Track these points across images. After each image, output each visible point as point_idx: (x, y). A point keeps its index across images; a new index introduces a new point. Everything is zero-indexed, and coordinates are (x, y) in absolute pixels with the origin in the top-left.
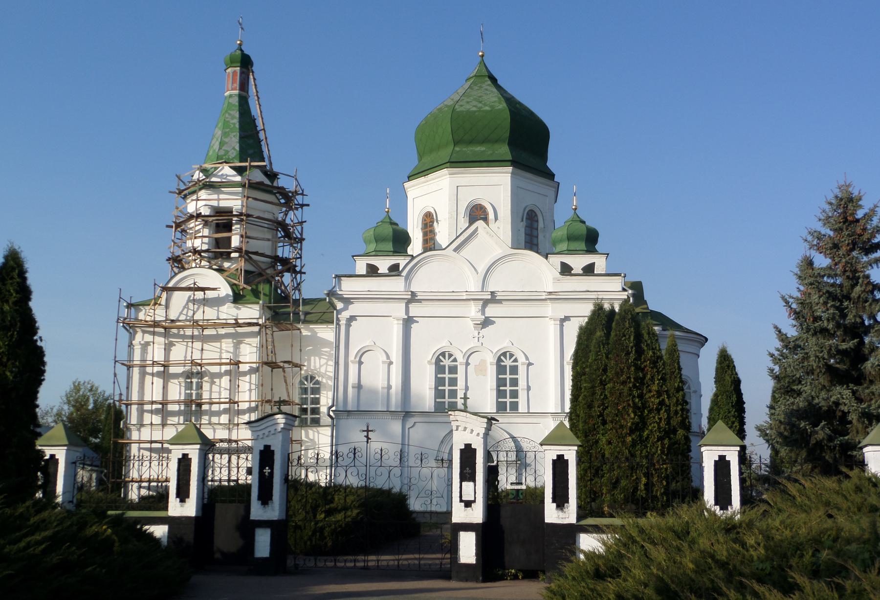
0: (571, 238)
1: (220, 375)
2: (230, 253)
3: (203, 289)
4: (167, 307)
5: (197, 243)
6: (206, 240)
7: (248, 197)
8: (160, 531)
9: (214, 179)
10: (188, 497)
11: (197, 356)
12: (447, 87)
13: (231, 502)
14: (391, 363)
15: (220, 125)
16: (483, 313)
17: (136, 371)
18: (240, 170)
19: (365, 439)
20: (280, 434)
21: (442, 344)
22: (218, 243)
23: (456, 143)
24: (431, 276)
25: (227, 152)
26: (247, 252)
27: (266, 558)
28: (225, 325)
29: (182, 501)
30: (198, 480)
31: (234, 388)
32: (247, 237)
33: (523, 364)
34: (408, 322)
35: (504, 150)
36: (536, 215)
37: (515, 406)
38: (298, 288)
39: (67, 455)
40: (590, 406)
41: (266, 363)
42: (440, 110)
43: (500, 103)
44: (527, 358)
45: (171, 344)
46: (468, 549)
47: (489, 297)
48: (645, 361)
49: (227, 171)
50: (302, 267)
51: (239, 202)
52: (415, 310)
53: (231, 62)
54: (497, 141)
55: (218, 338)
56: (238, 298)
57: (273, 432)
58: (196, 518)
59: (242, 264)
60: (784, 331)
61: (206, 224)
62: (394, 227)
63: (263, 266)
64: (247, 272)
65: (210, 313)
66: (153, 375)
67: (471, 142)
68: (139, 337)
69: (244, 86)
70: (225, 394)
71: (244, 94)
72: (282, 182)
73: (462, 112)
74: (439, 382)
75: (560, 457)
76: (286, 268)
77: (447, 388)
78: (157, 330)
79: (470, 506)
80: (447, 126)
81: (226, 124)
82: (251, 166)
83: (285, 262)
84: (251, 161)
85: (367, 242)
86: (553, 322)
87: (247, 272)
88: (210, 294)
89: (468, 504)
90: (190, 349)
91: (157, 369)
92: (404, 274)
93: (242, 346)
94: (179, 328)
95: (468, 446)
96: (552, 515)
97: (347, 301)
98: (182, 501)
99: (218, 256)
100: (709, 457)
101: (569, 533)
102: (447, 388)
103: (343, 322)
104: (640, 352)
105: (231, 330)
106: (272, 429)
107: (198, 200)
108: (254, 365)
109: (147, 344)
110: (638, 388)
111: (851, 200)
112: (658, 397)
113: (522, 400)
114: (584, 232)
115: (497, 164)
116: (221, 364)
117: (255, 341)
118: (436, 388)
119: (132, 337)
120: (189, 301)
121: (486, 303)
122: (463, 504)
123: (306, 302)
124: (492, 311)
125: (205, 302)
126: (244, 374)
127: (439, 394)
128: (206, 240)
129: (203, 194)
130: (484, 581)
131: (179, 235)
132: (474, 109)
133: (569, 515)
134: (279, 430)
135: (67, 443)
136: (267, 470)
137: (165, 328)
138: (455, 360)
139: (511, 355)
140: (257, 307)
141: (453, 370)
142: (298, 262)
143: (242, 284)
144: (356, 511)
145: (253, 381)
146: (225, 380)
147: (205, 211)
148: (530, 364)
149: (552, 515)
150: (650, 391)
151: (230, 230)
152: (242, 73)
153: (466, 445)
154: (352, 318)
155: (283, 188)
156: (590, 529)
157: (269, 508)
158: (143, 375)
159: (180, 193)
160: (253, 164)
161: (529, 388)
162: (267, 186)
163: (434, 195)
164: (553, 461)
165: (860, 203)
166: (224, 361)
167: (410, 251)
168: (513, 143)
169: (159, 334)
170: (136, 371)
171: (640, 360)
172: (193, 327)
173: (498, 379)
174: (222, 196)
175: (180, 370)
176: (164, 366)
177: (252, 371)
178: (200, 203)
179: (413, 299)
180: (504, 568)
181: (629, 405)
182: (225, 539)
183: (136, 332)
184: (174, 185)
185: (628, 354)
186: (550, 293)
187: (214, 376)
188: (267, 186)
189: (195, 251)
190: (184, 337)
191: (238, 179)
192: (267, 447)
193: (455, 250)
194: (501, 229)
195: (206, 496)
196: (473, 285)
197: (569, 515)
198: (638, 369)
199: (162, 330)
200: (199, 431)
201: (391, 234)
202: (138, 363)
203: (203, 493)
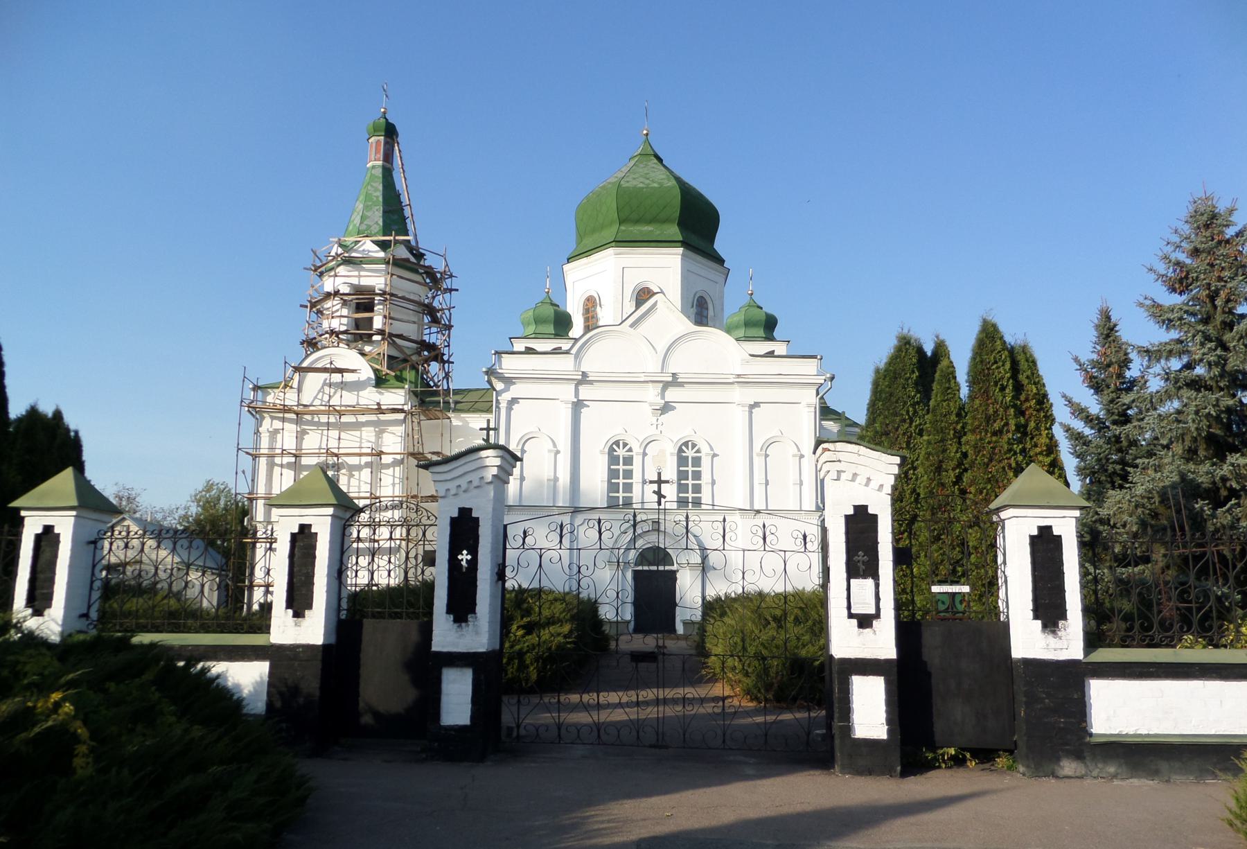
0: (748, 324)
1: (359, 468)
2: (372, 335)
4: (299, 390)
5: (336, 324)
6: (345, 321)
8: (246, 677)
9: (354, 255)
11: (333, 444)
12: (611, 167)
13: (397, 616)
14: (558, 452)
15: (362, 198)
16: (663, 397)
17: (263, 462)
18: (384, 245)
19: (655, 497)
20: (491, 487)
22: (358, 324)
24: (600, 357)
25: (369, 227)
26: (391, 335)
27: (463, 728)
28: (364, 411)
29: (298, 614)
30: (329, 575)
31: (375, 481)
32: (391, 318)
33: (707, 454)
34: (578, 405)
35: (674, 231)
37: (697, 503)
38: (447, 376)
40: (939, 469)
41: (412, 454)
42: (603, 188)
44: (712, 449)
45: (304, 432)
46: (869, 710)
47: (670, 379)
48: (1027, 400)
51: (382, 280)
52: (585, 392)
53: (375, 131)
55: (357, 426)
56: (380, 382)
57: (476, 483)
58: (324, 646)
59: (385, 348)
60: (1076, 400)
63: (408, 352)
65: (349, 398)
66: (282, 466)
67: (637, 221)
68: (267, 424)
69: (388, 157)
70: (366, 488)
72: (429, 261)
74: (613, 474)
75: (1045, 531)
76: (433, 353)
77: (621, 481)
78: (287, 415)
79: (870, 625)
80: (612, 203)
82: (397, 242)
83: (431, 347)
84: (397, 234)
85: (525, 324)
86: (740, 408)
88: (348, 377)
89: (865, 621)
90: (325, 438)
91: (286, 460)
92: (574, 351)
93: (385, 435)
94: (313, 413)
95: (861, 510)
96: (1028, 640)
97: (509, 381)
98: (298, 614)
99: (359, 338)
100: (1016, 532)
101: (1067, 682)
102: (621, 481)
103: (503, 405)
104: (1018, 388)
105: (373, 418)
106: (474, 477)
107: (336, 276)
108: (398, 457)
109: (276, 431)
110: (1020, 441)
111: (1214, 216)
112: (1048, 455)
113: (705, 497)
114: (764, 318)
116: (360, 455)
117: (400, 430)
119: (259, 423)
120: (324, 384)
121: (666, 385)
122: (855, 622)
123: (457, 392)
124: (672, 394)
125: (343, 386)
126: (387, 466)
127: (613, 487)
128: (345, 321)
129: (342, 270)
130: (905, 773)
131: (314, 316)
133: (1069, 643)
134: (489, 478)
135: (75, 503)
136: (464, 557)
137: (297, 414)
138: (630, 450)
139: (694, 446)
140: (402, 392)
141: (628, 461)
142: (446, 351)
143: (385, 370)
144: (566, 628)
145: (397, 475)
146: (366, 474)
147: (345, 289)
148: (715, 455)
149: (1028, 640)
150: (1036, 446)
151: (372, 311)
152: (386, 143)
153: (856, 507)
154: (514, 401)
155: (430, 267)
157: (468, 629)
158: (271, 466)
159: (315, 270)
161: (713, 483)
162: (412, 263)
163: (601, 277)
165: (929, 349)
166: (364, 451)
167: (571, 334)
168: (683, 224)
169: (290, 421)
170: (263, 462)
171: (1018, 399)
172: (328, 413)
173: (679, 472)
174: (362, 273)
175: (313, 461)
176: (295, 456)
177: (396, 463)
178: (339, 280)
179: (584, 379)
180: (933, 748)
181: (1010, 466)
182: (381, 686)
183: (263, 418)
184: (309, 261)
185: (1003, 389)
186: (739, 376)
187: (352, 468)
188: (412, 263)
189: (332, 332)
190: (319, 424)
191: (382, 254)
192: (465, 513)
193: (632, 326)
194: (669, 315)
195: (344, 605)
196: (651, 365)
197: (1069, 643)
198: (1020, 412)
199: (294, 416)
200: (333, 484)
202: (266, 451)
203: (340, 599)
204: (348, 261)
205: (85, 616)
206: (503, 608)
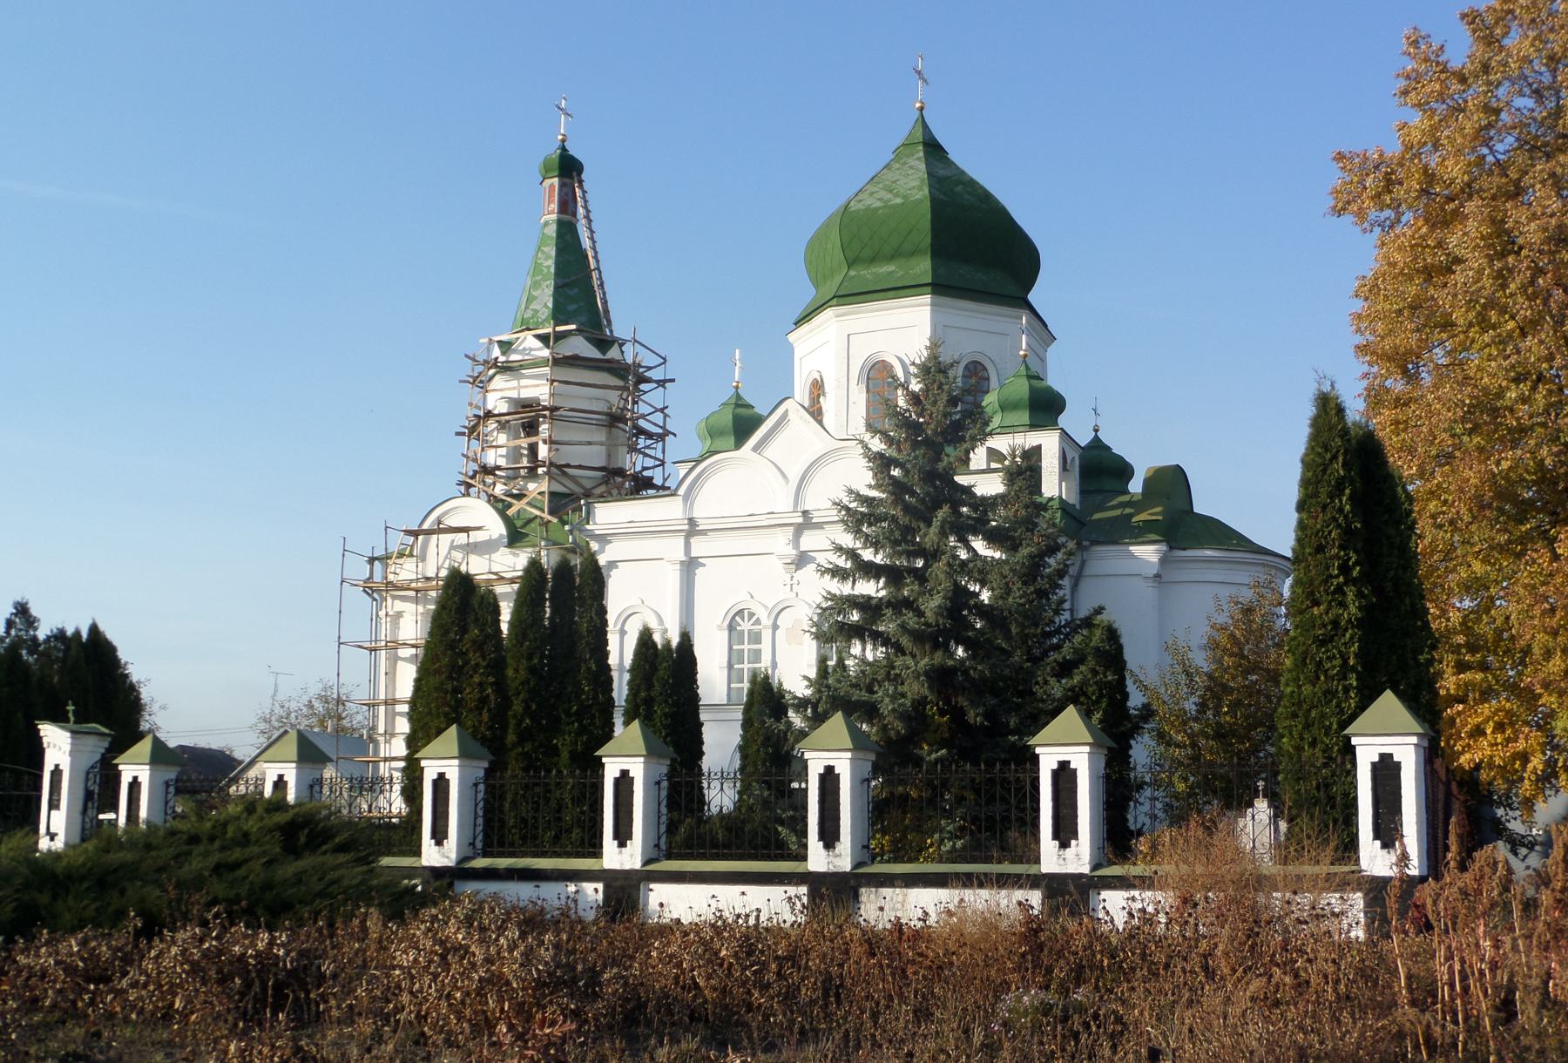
3: (465, 530)
7: (553, 381)
9: (513, 357)
10: (838, 838)
21: (739, 598)
23: (851, 264)
29: (622, 845)
34: (690, 566)
36: (985, 369)
39: (646, 770)
43: (920, 188)
47: (801, 520)
49: (530, 342)
50: (665, 480)
52: (699, 547)
54: (913, 254)
61: (503, 426)
62: (1035, 383)
64: (552, 494)
67: (873, 260)
69: (567, 205)
71: (567, 217)
73: (858, 211)
81: (537, 268)
87: (552, 494)
88: (475, 537)
92: (682, 491)
97: (604, 539)
115: (902, 292)
118: (730, 666)
121: (799, 530)
128: (503, 451)
132: (879, 204)
138: (758, 622)
141: (756, 638)
152: (562, 186)
156: (1137, 882)
160: (559, 329)
164: (1373, 764)
174: (524, 382)
179: (692, 529)
184: (467, 369)
191: (546, 353)
193: (755, 449)
201: (1026, 396)
204: (507, 369)
205: (866, 847)
206: (83, 829)
